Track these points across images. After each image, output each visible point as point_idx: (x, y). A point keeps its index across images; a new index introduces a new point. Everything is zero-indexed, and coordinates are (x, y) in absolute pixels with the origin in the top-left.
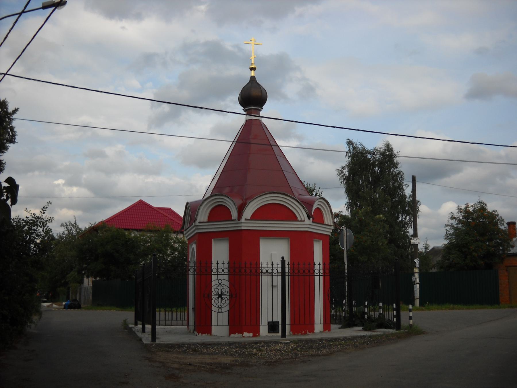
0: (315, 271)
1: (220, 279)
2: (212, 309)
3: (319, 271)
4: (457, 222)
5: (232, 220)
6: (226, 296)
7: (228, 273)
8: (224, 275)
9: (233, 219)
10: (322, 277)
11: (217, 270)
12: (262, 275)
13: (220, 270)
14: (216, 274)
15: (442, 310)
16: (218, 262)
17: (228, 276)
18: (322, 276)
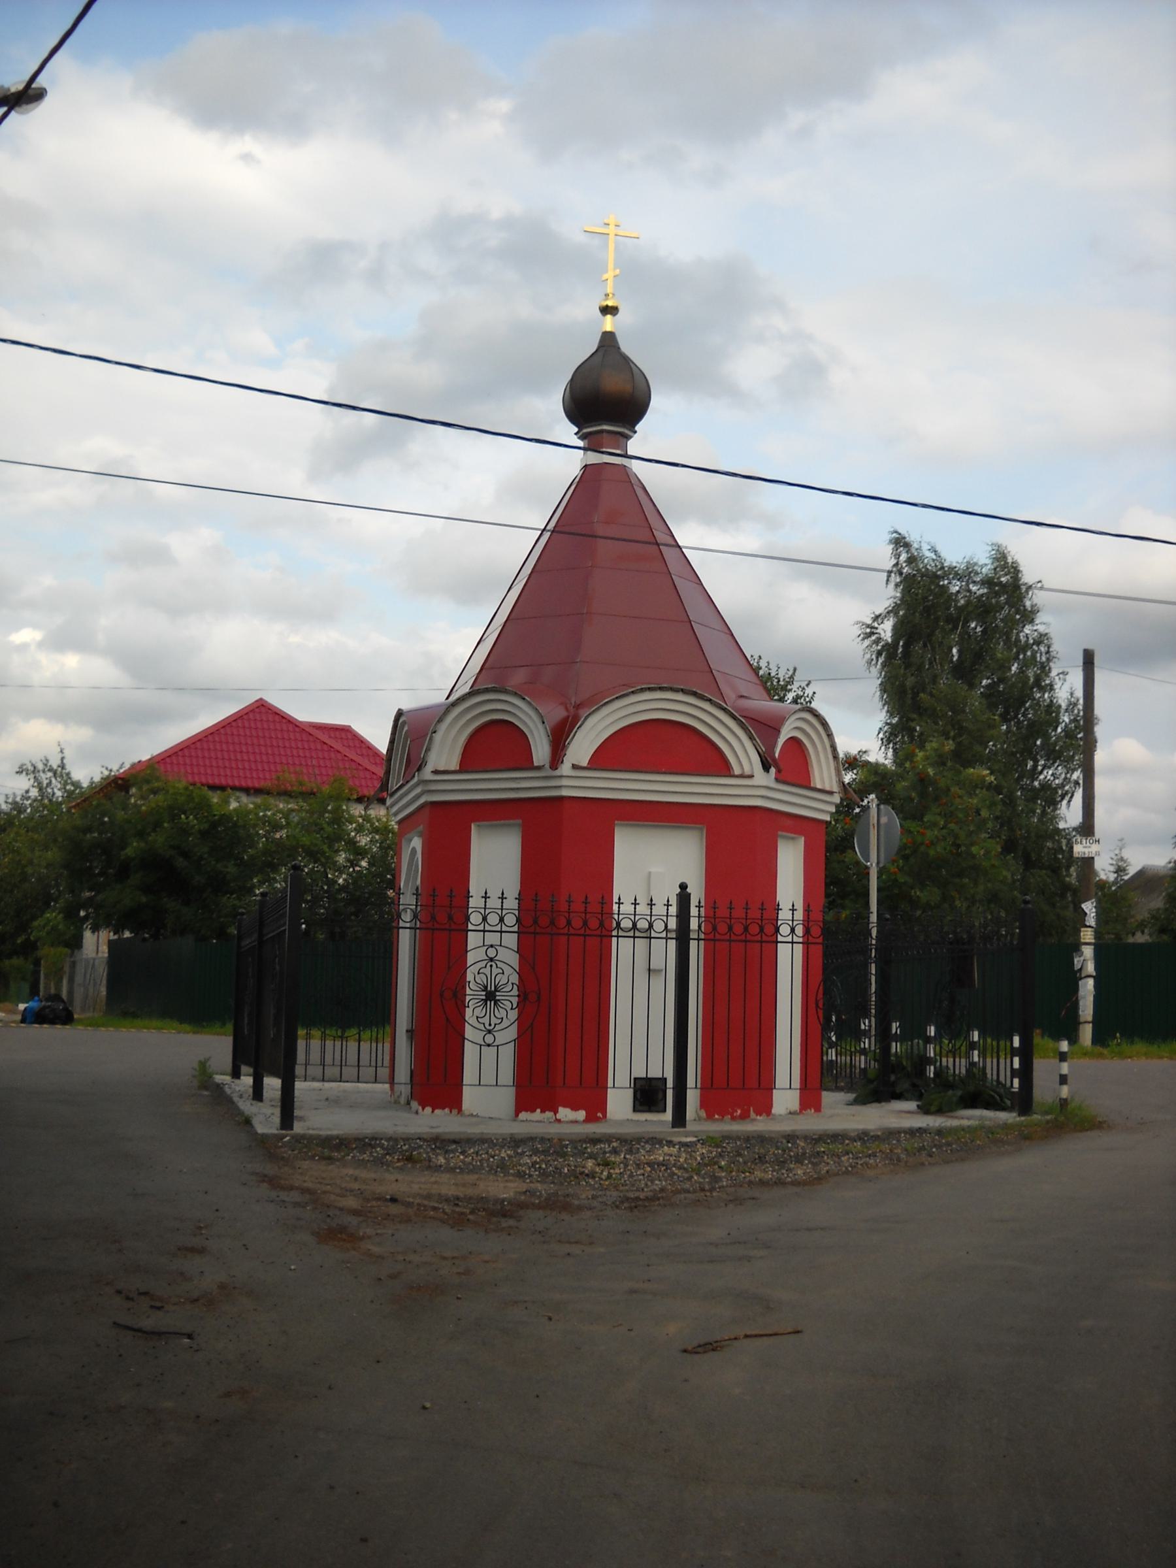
0: (781, 928)
1: (492, 946)
2: (466, 1037)
3: (793, 930)
5: (533, 768)
7: (516, 929)
9: (536, 764)
10: (799, 948)
11: (485, 919)
12: (618, 937)
13: (493, 919)
14: (498, 932)
17: (516, 935)
18: (801, 945)
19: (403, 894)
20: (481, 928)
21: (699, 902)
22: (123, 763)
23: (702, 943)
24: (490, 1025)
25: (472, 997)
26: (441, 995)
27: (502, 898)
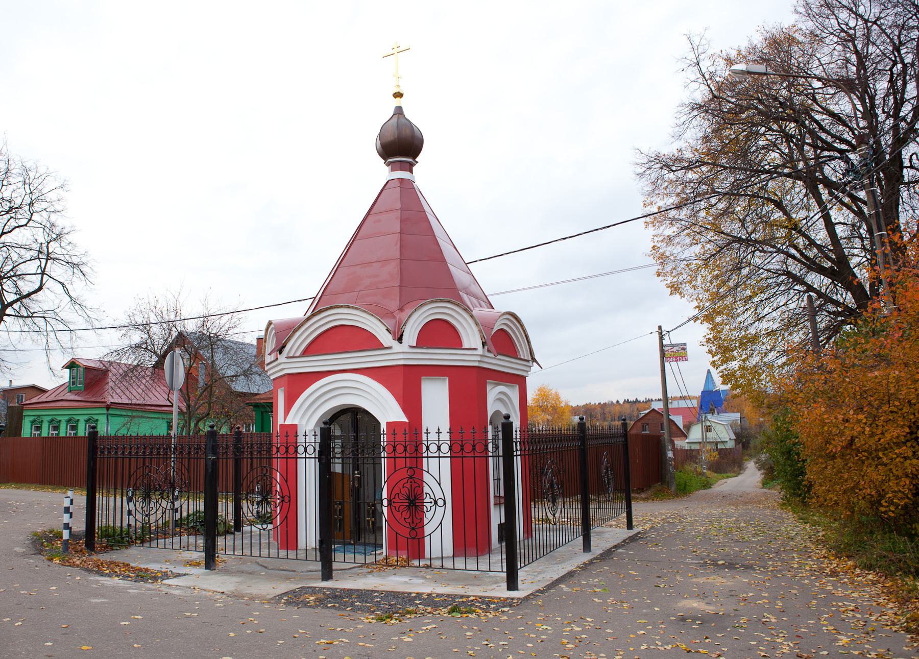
0: (448, 449)
4: (711, 336)
6: (401, 501)
7: (449, 454)
12: (428, 457)
15: (630, 537)
16: (439, 429)
20: (437, 455)
22: (660, 327)
23: (386, 459)
25: (401, 504)
26: (445, 501)
27: (439, 433)
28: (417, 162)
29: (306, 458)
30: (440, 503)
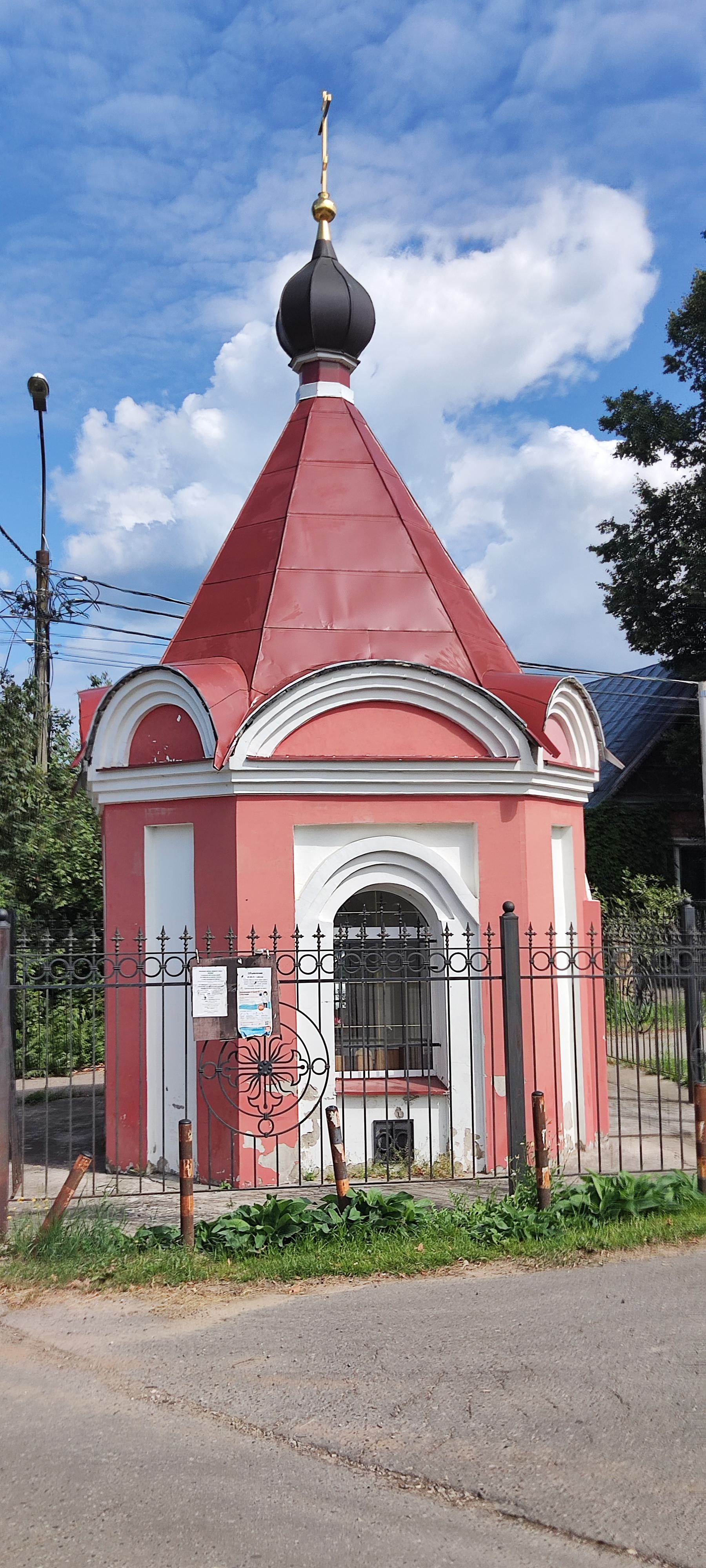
3: (319, 965)
8: (473, 978)
13: (308, 964)
16: (319, 930)
19: (596, 934)
20: (315, 976)
21: (186, 932)
24: (265, 1107)
28: (358, 363)
29: (319, 981)
30: (319, 1067)
